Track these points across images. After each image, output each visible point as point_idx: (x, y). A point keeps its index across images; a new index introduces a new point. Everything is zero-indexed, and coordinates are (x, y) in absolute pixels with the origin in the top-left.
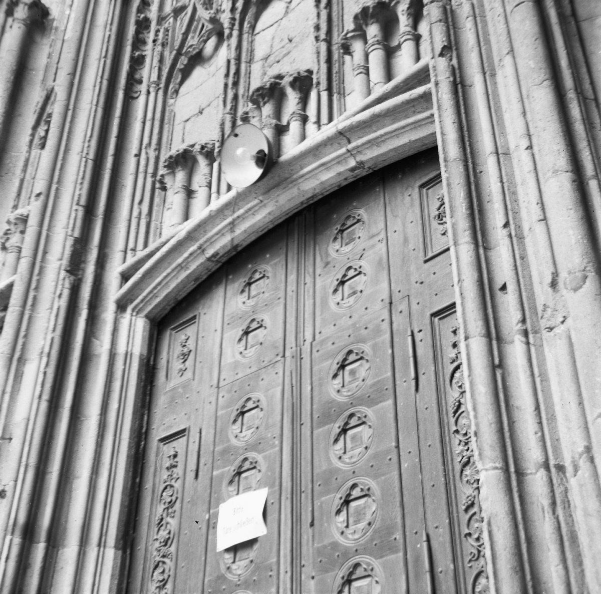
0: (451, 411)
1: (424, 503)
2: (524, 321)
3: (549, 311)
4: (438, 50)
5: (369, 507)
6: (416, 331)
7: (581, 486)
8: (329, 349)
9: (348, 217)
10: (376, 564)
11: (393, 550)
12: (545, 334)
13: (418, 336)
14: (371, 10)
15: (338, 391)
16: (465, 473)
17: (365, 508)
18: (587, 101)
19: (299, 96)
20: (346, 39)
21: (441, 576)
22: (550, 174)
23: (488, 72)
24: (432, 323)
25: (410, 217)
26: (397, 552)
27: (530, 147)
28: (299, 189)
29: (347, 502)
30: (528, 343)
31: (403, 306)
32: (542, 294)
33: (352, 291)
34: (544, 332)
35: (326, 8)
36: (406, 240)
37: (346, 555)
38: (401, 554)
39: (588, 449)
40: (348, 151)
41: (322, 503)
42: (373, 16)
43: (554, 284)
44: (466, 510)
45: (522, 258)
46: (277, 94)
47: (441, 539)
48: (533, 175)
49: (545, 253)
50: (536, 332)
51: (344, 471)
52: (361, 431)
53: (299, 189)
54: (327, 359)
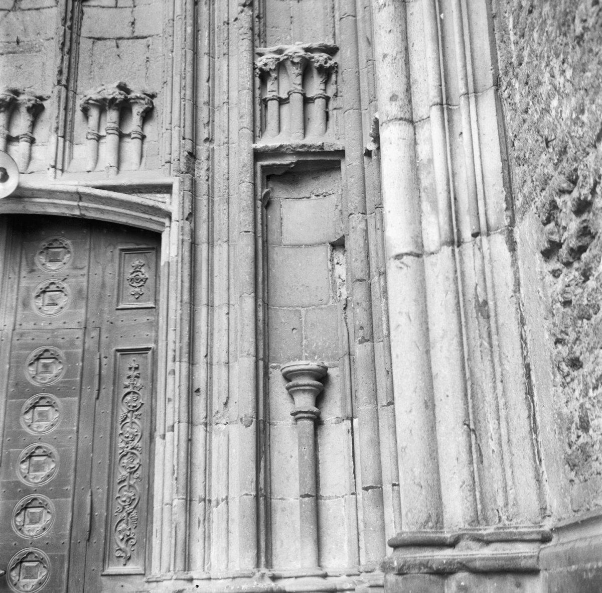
0: (120, 420)
1: (91, 472)
2: (206, 418)
3: (219, 415)
4: (186, 215)
5: (49, 465)
6: (103, 356)
7: (219, 513)
8: (29, 342)
9: (56, 240)
10: (49, 501)
11: (64, 494)
12: (214, 426)
13: (104, 361)
14: (117, 102)
15: (33, 377)
16: (122, 461)
17: (44, 463)
18: (191, 138)
19: (31, 119)
20: (88, 103)
21: (97, 518)
22: (245, 354)
23: (211, 243)
24: (115, 356)
25: (109, 269)
26: (67, 497)
27: (228, 314)
28: (24, 207)
29: (30, 457)
30: (206, 431)
31: (95, 334)
32: (217, 405)
33: (51, 302)
34: (214, 425)
35: (68, 53)
36: (103, 286)
37: (27, 491)
38: (70, 499)
39: (227, 497)
40: (79, 205)
41: (9, 453)
42: (117, 105)
43: (226, 404)
44: (119, 483)
45: (211, 378)
46: (11, 107)
47: (100, 496)
48: (227, 332)
49: (224, 383)
50: (211, 425)
51: (32, 436)
52: (47, 411)
53: (24, 207)
54: (26, 349)
